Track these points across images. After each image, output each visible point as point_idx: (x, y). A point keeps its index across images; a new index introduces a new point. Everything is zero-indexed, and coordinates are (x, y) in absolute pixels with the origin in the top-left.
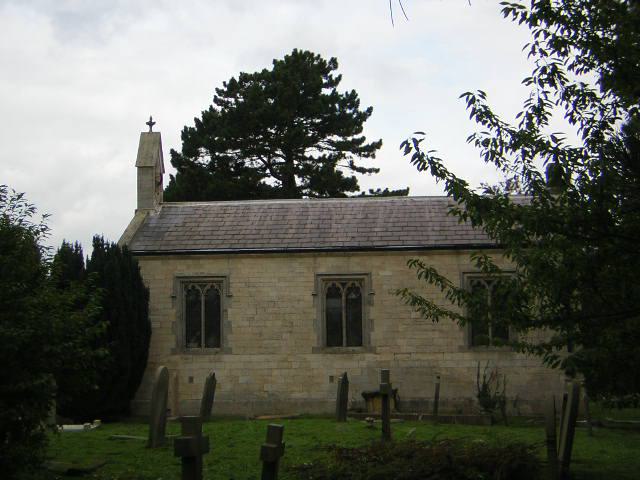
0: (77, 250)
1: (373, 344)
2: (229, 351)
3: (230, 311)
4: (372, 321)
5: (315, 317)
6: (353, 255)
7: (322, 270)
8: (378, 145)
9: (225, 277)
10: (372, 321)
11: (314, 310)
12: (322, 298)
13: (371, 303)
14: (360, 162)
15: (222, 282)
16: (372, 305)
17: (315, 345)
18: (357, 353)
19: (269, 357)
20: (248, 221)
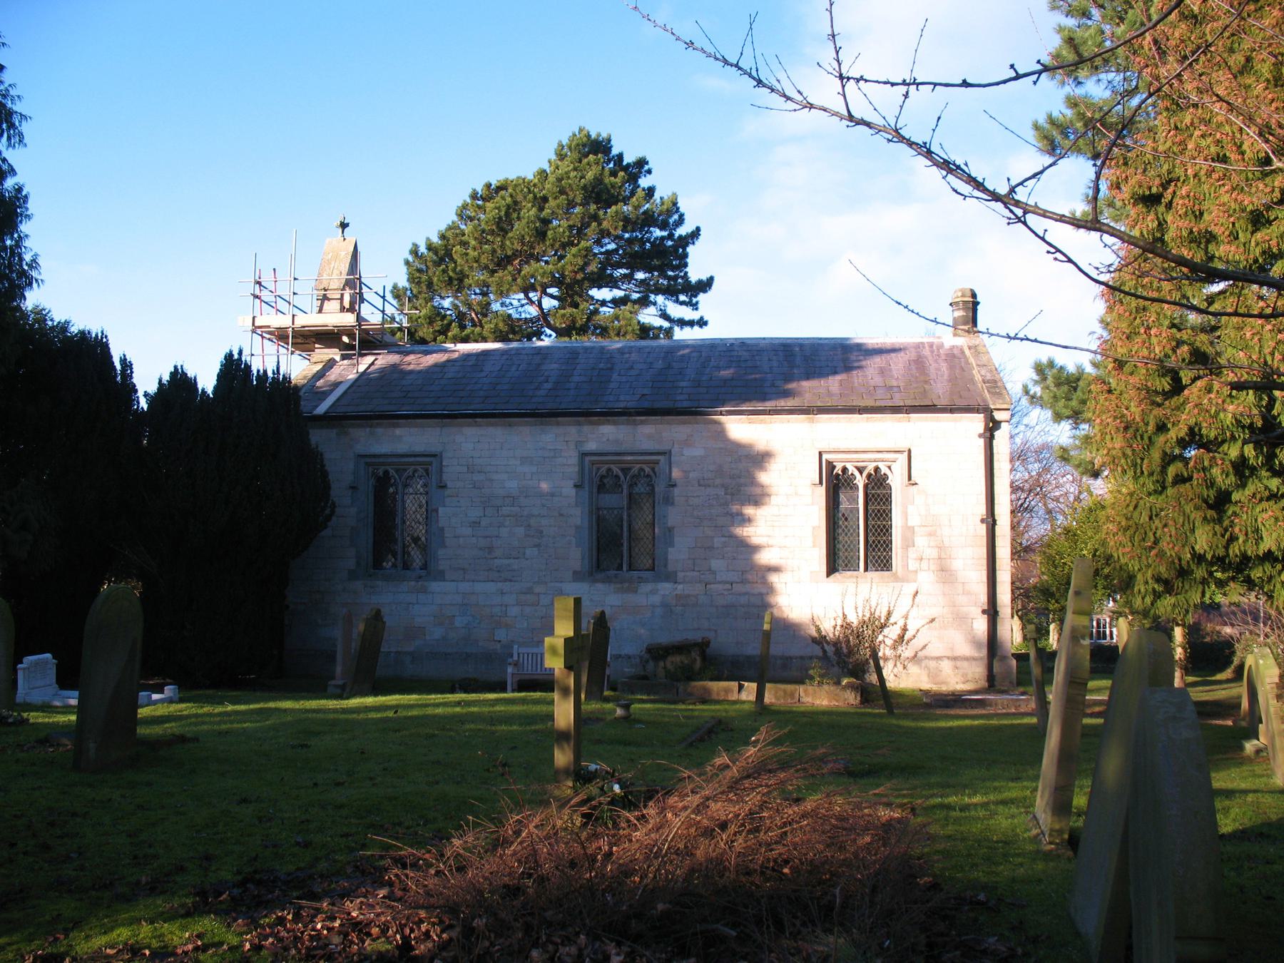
0: (102, 338)
1: (670, 568)
2: (441, 576)
3: (441, 510)
4: (670, 530)
5: (579, 523)
6: (642, 422)
7: (592, 446)
8: (705, 285)
9: (434, 456)
10: (670, 530)
11: (578, 512)
12: (591, 493)
13: (668, 501)
14: (676, 311)
15: (430, 463)
16: (673, 504)
17: (579, 569)
18: (647, 581)
19: (506, 586)
20: (482, 371)
